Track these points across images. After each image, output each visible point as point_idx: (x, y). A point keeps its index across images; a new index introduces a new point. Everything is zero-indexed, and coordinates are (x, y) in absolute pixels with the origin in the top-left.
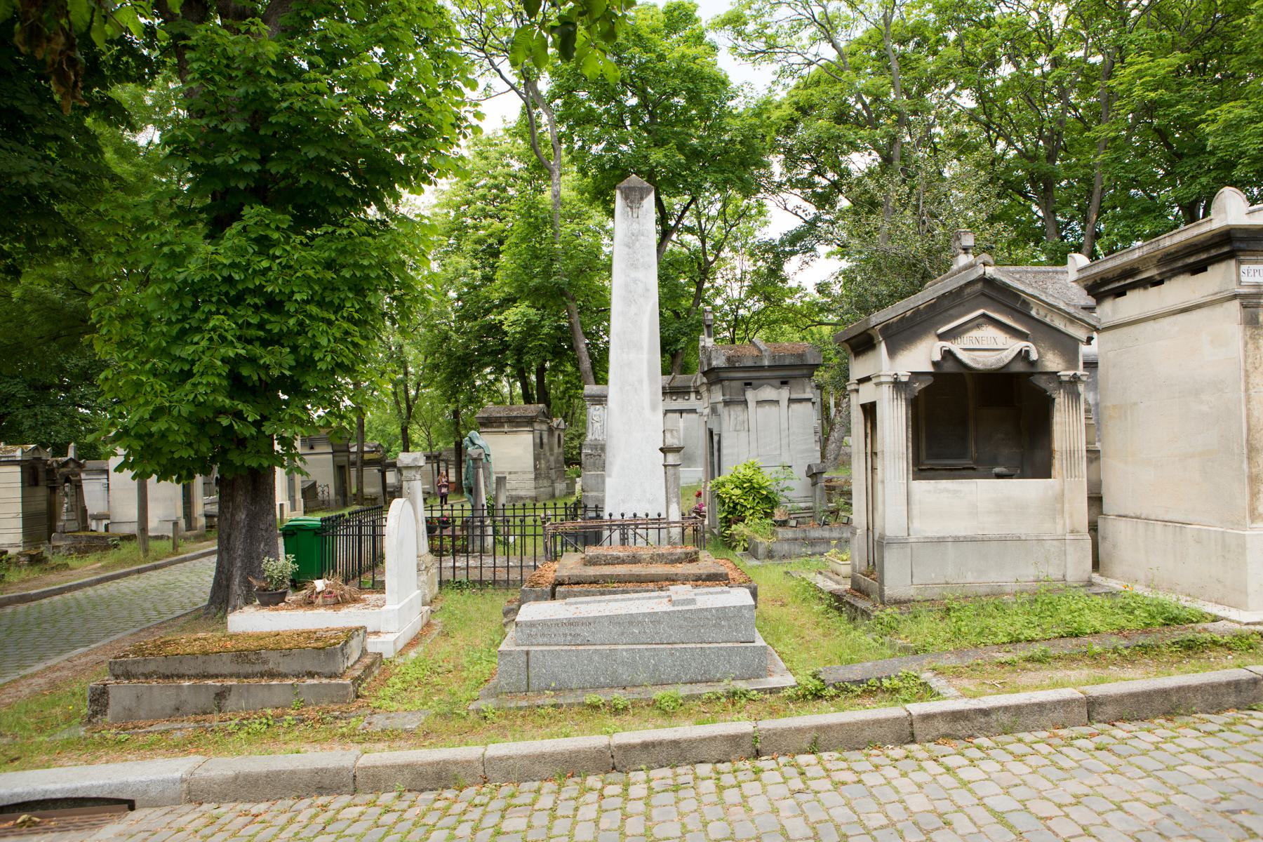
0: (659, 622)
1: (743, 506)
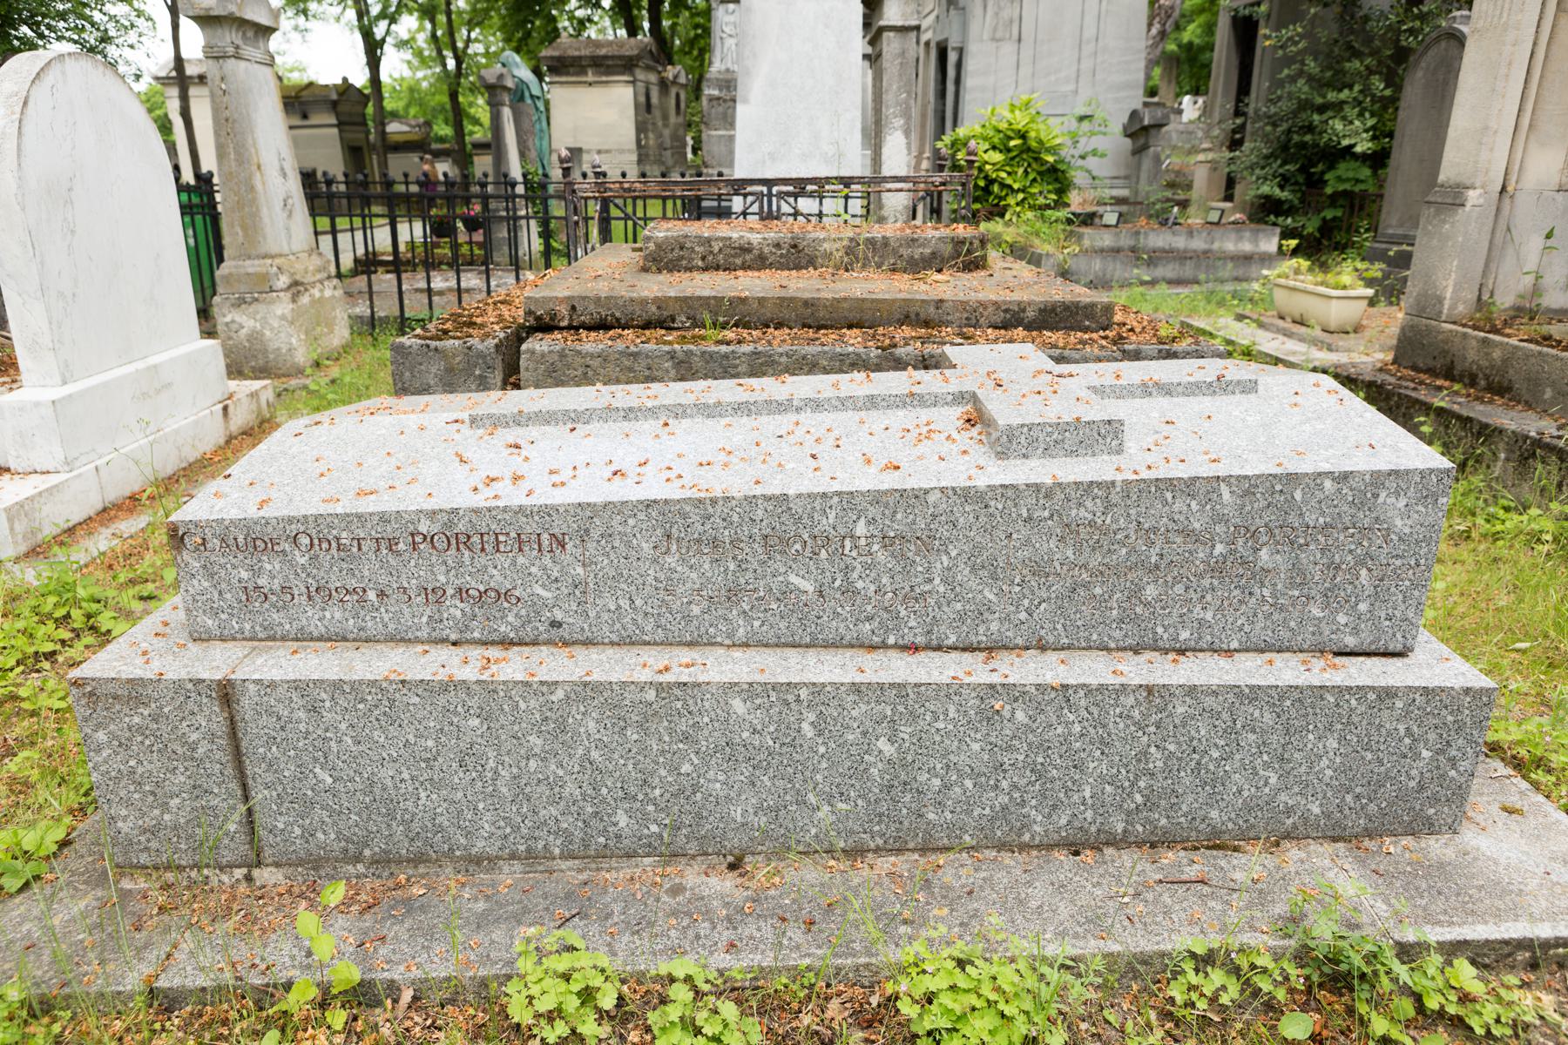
0: (928, 543)
1: (1003, 186)
